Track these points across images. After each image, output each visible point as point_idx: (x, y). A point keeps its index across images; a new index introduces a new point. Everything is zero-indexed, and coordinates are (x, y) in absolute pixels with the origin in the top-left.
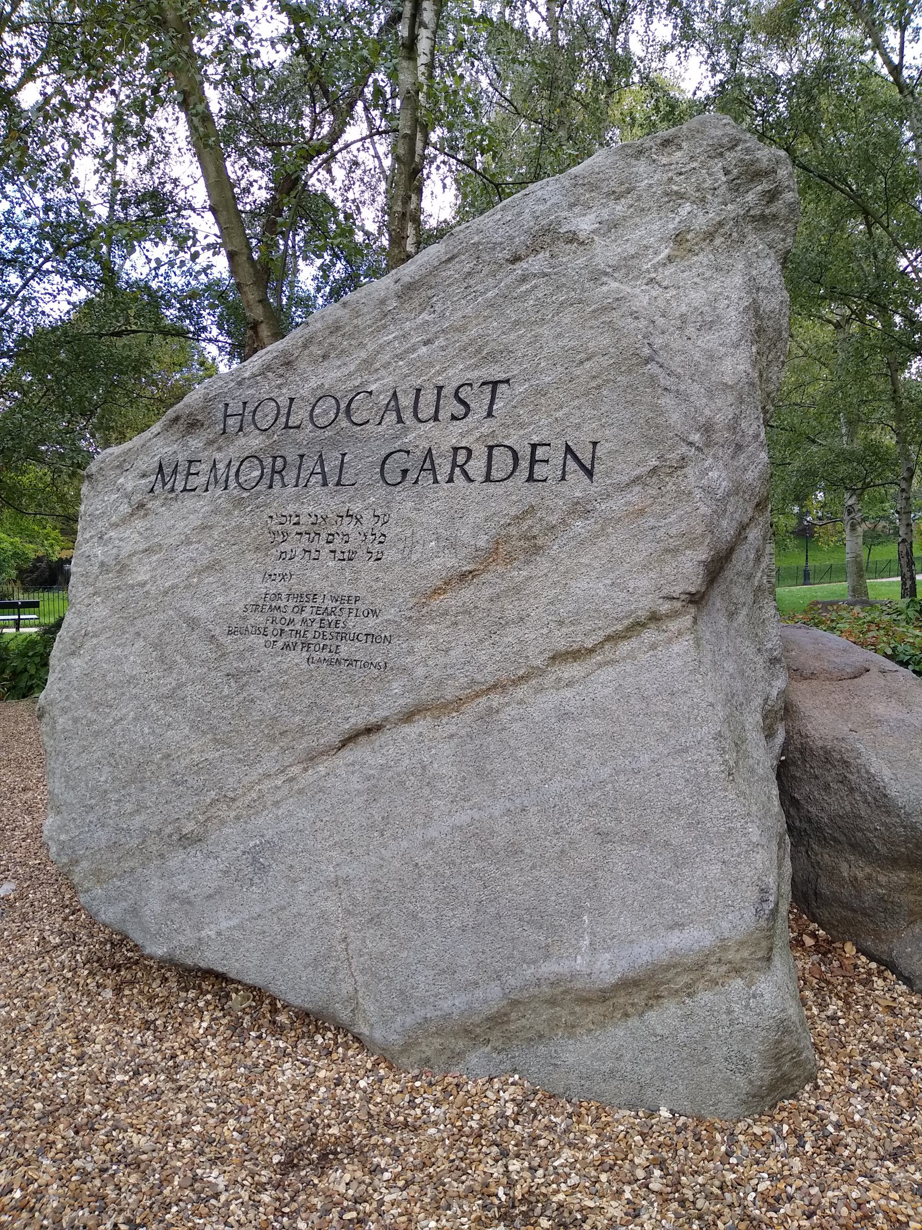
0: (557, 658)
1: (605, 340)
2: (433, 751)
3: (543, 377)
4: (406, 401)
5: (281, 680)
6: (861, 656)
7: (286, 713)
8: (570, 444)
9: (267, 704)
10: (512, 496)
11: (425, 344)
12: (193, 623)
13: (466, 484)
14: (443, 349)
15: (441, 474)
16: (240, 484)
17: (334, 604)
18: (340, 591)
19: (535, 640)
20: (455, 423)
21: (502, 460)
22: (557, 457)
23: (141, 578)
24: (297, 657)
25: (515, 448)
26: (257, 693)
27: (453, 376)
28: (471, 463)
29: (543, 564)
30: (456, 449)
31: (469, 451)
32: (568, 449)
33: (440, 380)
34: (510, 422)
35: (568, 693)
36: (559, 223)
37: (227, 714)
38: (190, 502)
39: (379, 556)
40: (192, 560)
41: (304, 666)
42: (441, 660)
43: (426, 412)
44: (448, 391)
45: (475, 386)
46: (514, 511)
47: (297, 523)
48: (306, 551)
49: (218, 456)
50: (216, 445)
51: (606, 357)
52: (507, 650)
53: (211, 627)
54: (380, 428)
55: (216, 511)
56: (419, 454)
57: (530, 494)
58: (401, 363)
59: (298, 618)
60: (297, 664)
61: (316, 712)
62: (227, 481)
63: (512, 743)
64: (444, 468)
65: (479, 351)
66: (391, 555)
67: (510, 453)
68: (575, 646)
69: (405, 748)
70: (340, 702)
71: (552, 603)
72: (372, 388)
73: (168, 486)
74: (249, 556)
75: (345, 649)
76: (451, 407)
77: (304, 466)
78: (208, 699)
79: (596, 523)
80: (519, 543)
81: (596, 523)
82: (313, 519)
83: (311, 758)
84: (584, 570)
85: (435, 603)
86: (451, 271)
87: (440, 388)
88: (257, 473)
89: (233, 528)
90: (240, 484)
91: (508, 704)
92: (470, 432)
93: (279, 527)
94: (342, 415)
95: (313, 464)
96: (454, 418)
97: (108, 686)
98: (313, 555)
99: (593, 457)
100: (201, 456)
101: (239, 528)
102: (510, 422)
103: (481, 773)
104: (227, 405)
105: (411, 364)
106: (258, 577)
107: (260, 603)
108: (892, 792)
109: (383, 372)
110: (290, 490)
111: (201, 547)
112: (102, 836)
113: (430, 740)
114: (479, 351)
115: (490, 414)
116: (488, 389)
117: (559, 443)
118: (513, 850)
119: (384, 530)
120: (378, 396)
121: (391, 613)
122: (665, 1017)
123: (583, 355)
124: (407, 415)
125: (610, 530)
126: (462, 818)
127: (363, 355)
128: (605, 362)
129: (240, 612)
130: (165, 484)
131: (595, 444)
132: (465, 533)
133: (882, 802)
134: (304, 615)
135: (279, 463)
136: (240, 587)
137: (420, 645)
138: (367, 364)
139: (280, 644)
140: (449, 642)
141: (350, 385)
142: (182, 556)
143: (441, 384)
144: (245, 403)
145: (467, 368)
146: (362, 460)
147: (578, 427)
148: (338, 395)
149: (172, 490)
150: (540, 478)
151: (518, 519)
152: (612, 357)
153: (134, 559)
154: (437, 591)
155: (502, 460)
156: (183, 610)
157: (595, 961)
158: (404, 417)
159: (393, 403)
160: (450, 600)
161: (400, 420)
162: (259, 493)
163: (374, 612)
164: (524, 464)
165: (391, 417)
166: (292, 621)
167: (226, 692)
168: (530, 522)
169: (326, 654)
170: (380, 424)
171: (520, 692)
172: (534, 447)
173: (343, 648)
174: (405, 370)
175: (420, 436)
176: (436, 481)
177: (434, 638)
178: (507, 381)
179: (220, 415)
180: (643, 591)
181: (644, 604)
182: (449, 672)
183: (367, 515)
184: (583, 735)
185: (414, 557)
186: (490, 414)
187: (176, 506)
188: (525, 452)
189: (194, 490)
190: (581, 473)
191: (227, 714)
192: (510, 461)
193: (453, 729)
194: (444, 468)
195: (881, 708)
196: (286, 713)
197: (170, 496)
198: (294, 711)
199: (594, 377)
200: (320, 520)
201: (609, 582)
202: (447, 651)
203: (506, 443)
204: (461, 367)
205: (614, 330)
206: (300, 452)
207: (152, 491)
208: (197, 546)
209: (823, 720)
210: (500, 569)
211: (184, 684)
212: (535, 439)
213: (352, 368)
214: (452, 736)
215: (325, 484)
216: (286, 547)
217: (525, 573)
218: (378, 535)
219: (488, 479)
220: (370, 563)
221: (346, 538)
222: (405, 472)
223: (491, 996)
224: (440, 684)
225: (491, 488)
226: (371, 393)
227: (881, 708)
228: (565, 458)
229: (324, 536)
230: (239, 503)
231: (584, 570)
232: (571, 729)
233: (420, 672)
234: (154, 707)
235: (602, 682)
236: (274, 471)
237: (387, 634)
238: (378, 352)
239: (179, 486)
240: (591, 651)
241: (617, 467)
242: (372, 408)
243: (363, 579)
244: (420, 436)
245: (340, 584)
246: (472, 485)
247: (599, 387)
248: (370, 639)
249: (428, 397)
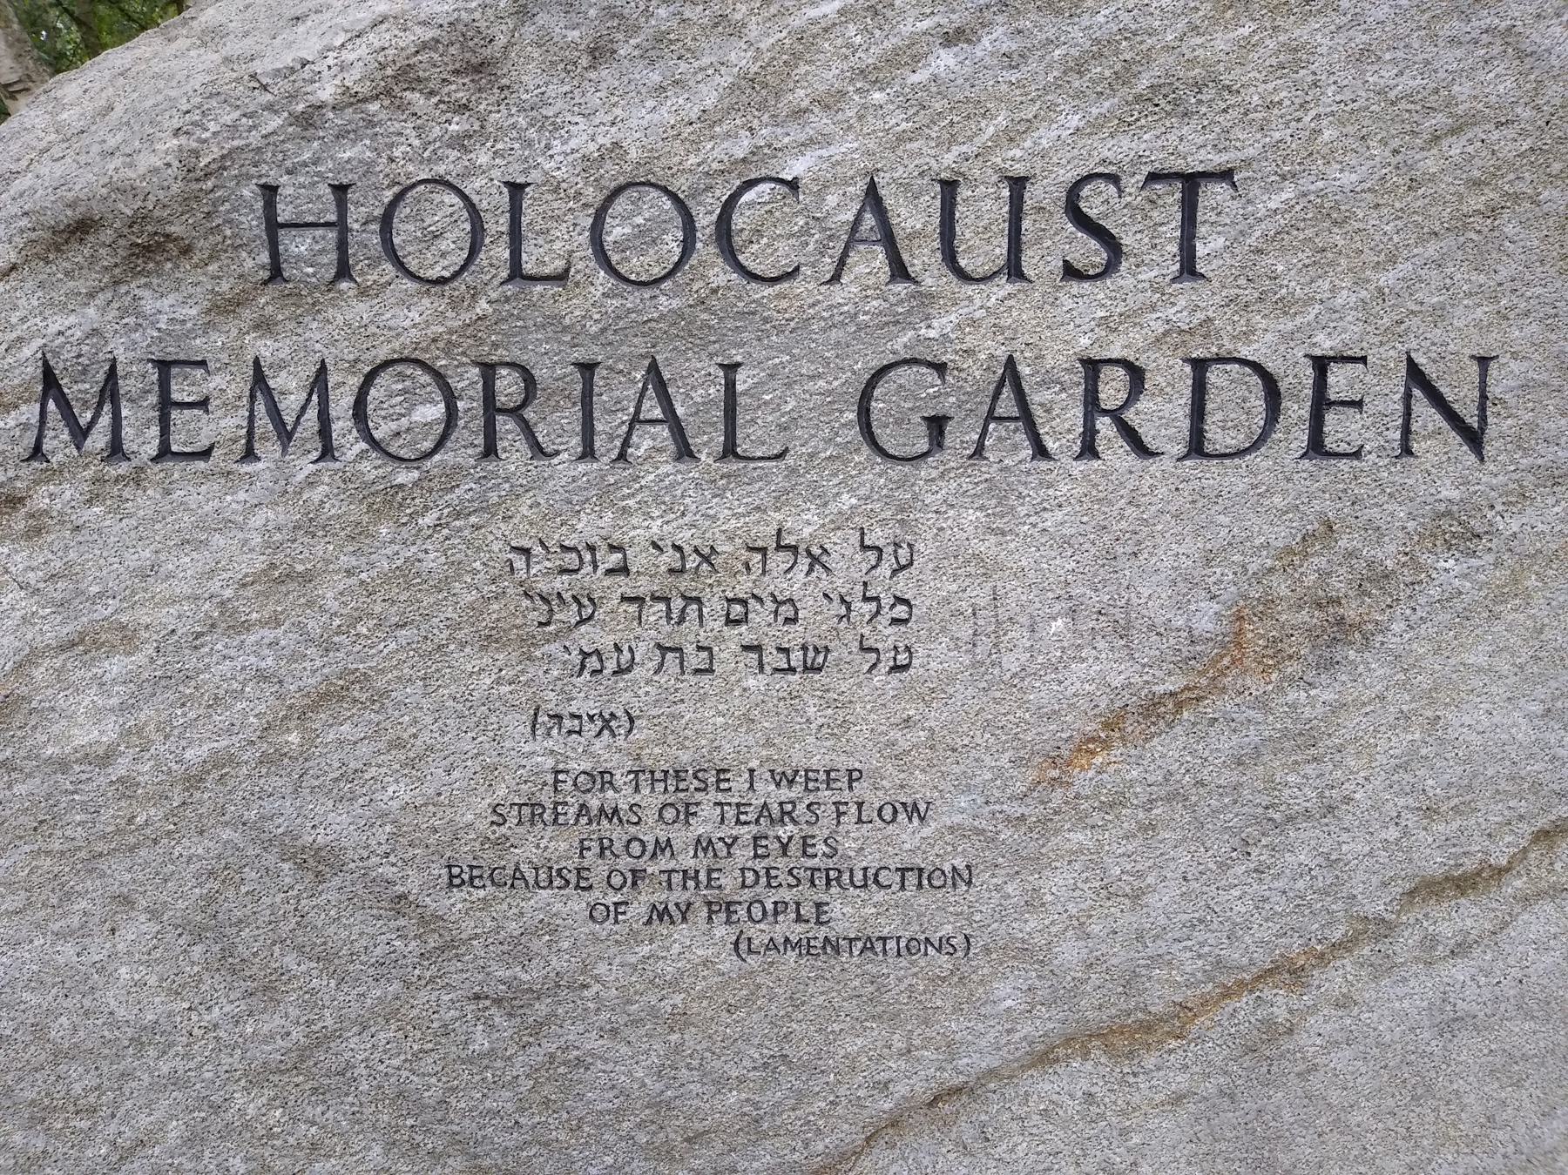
0: (1428, 889)
1: (1501, 83)
2: (1136, 1139)
3: (1333, 171)
4: (914, 217)
5: (666, 1006)
7: (696, 1088)
8: (1420, 359)
10: (1268, 495)
11: (951, 38)
12: (319, 863)
13: (1132, 460)
14: (1010, 60)
15: (1057, 435)
16: (375, 444)
17: (785, 793)
18: (798, 759)
20: (1075, 287)
21: (1234, 405)
22: (1386, 393)
23: (85, 735)
25: (1270, 366)
26: (593, 1043)
27: (1058, 147)
28: (1144, 404)
30: (1092, 367)
31: (1136, 374)
32: (1415, 374)
33: (1015, 159)
34: (1250, 294)
35: (1459, 971)
37: (502, 1100)
38: (195, 494)
39: (902, 658)
40: (262, 676)
41: (728, 963)
42: (1128, 920)
43: (982, 247)
44: (1045, 193)
45: (1132, 183)
46: (1280, 535)
47: (624, 570)
48: (664, 650)
49: (265, 348)
50: (247, 314)
51: (1510, 132)
52: (1300, 884)
53: (388, 871)
54: (838, 294)
55: (310, 526)
56: (977, 373)
58: (878, 97)
59: (681, 837)
60: (706, 963)
61: (789, 1079)
62: (325, 431)
63: (1334, 1096)
64: (1062, 421)
65: (1125, 76)
66: (936, 657)
67: (1255, 380)
68: (1470, 865)
69: (1057, 1137)
70: (853, 1045)
71: (1404, 767)
72: (796, 167)
73: (98, 440)
74: (468, 659)
76: (1053, 242)
77: (602, 400)
78: (427, 1065)
79: (1497, 564)
81: (1497, 564)
82: (669, 558)
84: (1476, 683)
87: (1018, 185)
88: (433, 412)
89: (386, 579)
90: (375, 444)
91: (1313, 1009)
92: (1137, 315)
93: (561, 583)
94: (706, 250)
95: (632, 393)
96: (1071, 272)
97: (58, 1056)
98: (695, 660)
99: (1484, 397)
100: (199, 346)
101: (406, 575)
102: (1250, 294)
104: (270, 191)
105: (913, 102)
106: (517, 724)
107: (546, 797)
109: (820, 121)
110: (566, 468)
111: (287, 638)
113: (1122, 1113)
114: (1125, 76)
115: (1188, 268)
116: (1171, 196)
117: (1389, 357)
119: (902, 585)
120: (820, 195)
121: (957, 809)
123: (1440, 120)
124: (923, 258)
125: (1532, 581)
127: (739, 57)
128: (1508, 144)
129: (482, 825)
130: (80, 434)
131: (1483, 361)
132: (1151, 596)
134: (699, 828)
135: (508, 386)
137: (1056, 883)
138: (757, 91)
139: (638, 910)
140: (1140, 875)
141: (716, 152)
142: (223, 664)
143: (1019, 170)
144: (340, 190)
145: (1095, 126)
146: (795, 393)
147: (1438, 315)
148: (681, 185)
149: (116, 450)
150: (1344, 447)
151: (1290, 557)
152: (1523, 133)
153: (38, 673)
154: (1088, 745)
155: (1234, 405)
156: (279, 827)
158: (915, 265)
159: (869, 220)
160: (1116, 768)
161: (900, 271)
162: (453, 475)
163: (913, 810)
164: (1297, 410)
165: (870, 263)
166: (663, 847)
167: (481, 1042)
168: (1320, 562)
169: (785, 927)
170: (836, 278)
171: (1334, 979)
172: (1321, 365)
173: (836, 909)
174: (899, 121)
175: (971, 323)
176: (1041, 452)
177: (1096, 864)
178: (1226, 175)
179: (251, 222)
182: (1161, 947)
183: (842, 547)
184: (1499, 1060)
185: (1011, 662)
186: (1188, 268)
187: (144, 502)
188: (1297, 379)
189: (205, 454)
190: (1454, 438)
191: (502, 1100)
192: (1258, 403)
193: (1181, 1081)
194: (1062, 421)
196: (696, 1088)
197: (112, 471)
198: (722, 1083)
199: (1477, 183)
200: (692, 562)
201: (1536, 708)
202: (1136, 896)
203: (1245, 352)
204: (1075, 121)
205: (1521, 55)
206: (579, 355)
207: (37, 452)
208: (269, 634)
210: (1256, 685)
211: (337, 1034)
212: (1325, 344)
213: (709, 97)
214: (1178, 1099)
215: (685, 452)
216: (588, 636)
217: (1328, 696)
218: (886, 601)
219: (1197, 446)
220: (878, 678)
221: (786, 611)
222: (937, 425)
224: (1131, 981)
225: (1209, 474)
226: (793, 185)
228: (1408, 396)
229: (714, 605)
230: (389, 500)
231: (1476, 683)
232: (1469, 1049)
233: (1070, 953)
234: (247, 1104)
236: (491, 407)
237: (960, 863)
238: (797, 57)
239: (142, 440)
240: (1500, 872)
242: (805, 231)
243: (856, 718)
244: (971, 323)
245: (793, 737)
246: (1154, 466)
247: (1493, 212)
248: (912, 878)
249: (982, 211)
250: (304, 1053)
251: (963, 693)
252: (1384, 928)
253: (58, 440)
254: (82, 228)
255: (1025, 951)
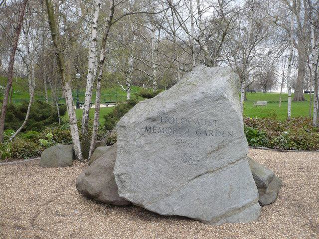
12: (161, 158)
36: (57, 230)
49: (160, 126)
83: (190, 181)
85: (209, 155)
108: (131, 200)
171: (225, 169)
194: (208, 134)
250: (159, 170)
251: (202, 150)
252: (227, 166)
253: (146, 131)
254: (150, 119)
255: (205, 166)
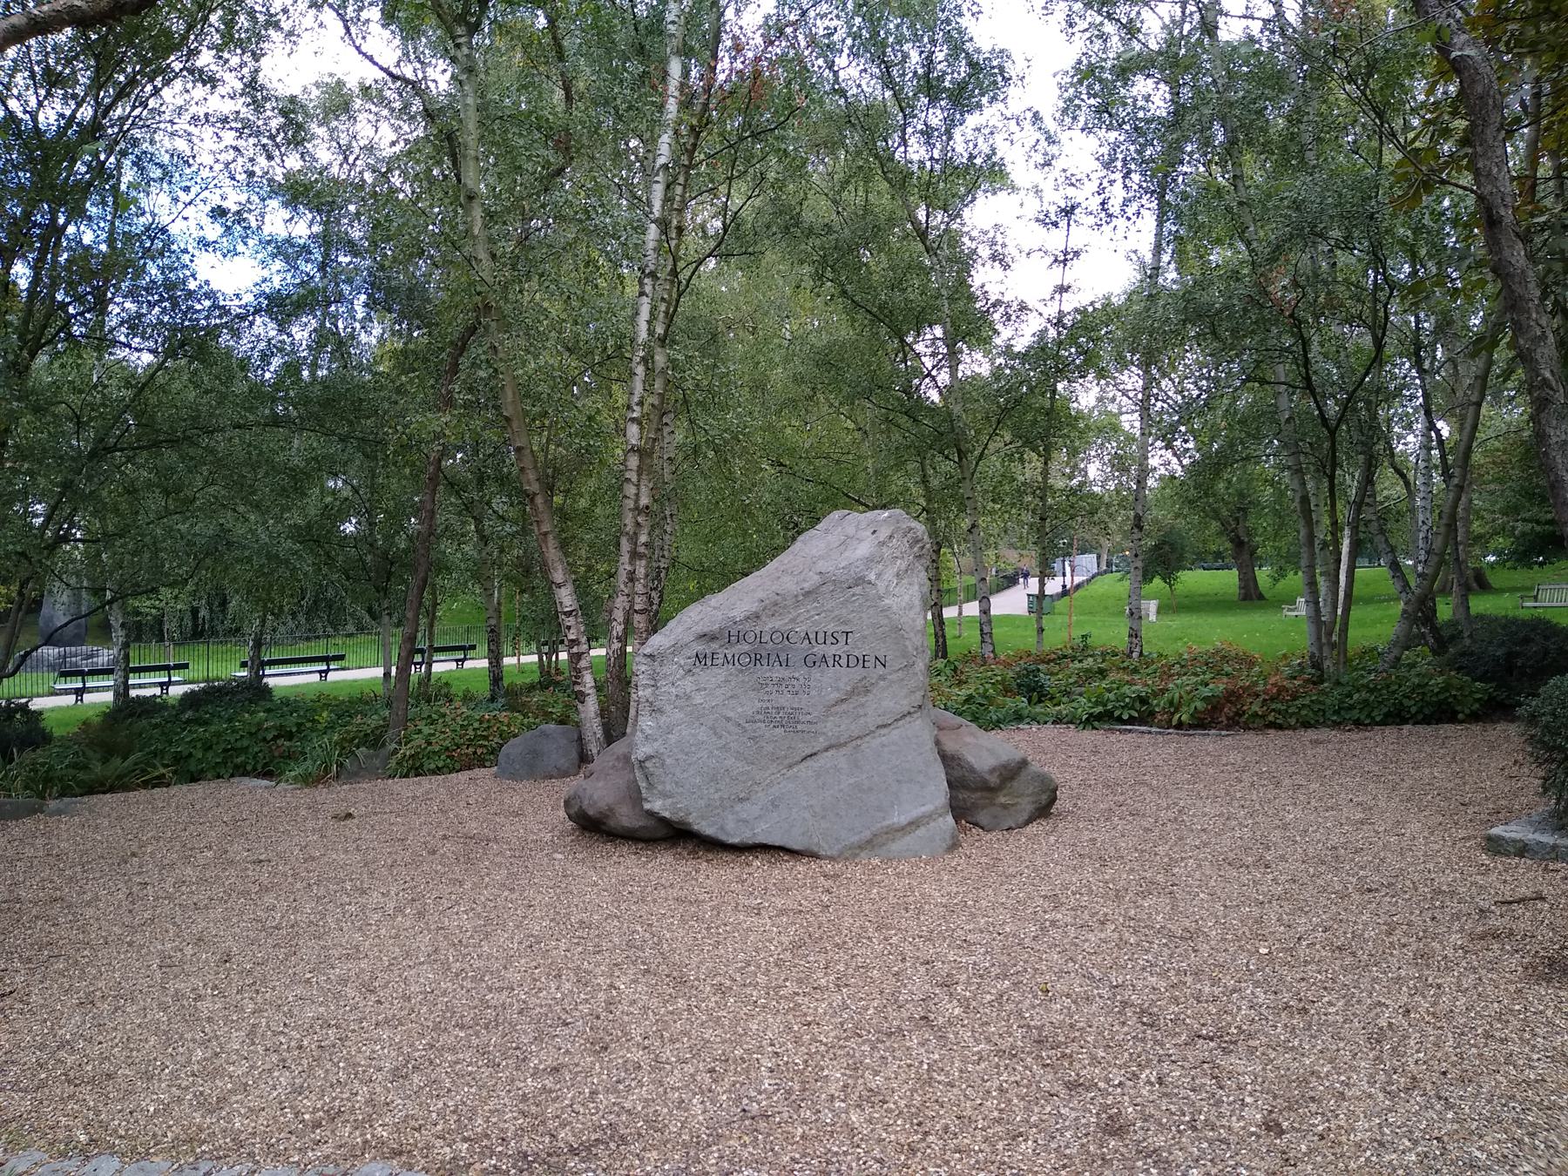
6: (959, 720)
9: (770, 748)
10: (857, 673)
12: (728, 719)
19: (872, 721)
24: (780, 731)
27: (831, 628)
29: (871, 696)
57: (864, 672)
64: (831, 663)
66: (813, 693)
75: (799, 727)
76: (830, 640)
80: (861, 689)
83: (790, 767)
86: (824, 588)
103: (857, 766)
112: (702, 803)
118: (870, 789)
122: (921, 832)
126: (852, 781)
132: (842, 685)
133: (972, 770)
136: (749, 705)
138: (793, 620)
155: (853, 661)
157: (898, 819)
175: (819, 649)
180: (905, 705)
181: (906, 709)
194: (831, 663)
195: (968, 739)
209: (950, 746)
223: (867, 834)
227: (968, 739)
235: (894, 734)
241: (894, 664)
249: (821, 636)
